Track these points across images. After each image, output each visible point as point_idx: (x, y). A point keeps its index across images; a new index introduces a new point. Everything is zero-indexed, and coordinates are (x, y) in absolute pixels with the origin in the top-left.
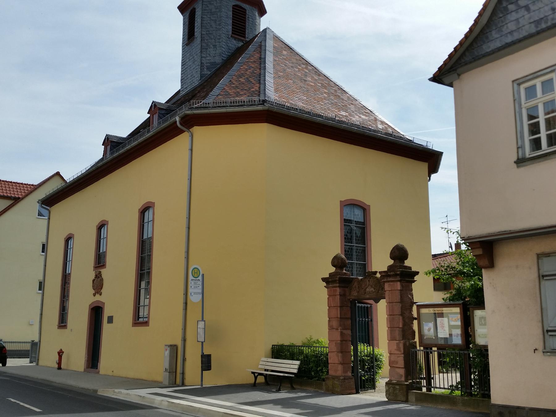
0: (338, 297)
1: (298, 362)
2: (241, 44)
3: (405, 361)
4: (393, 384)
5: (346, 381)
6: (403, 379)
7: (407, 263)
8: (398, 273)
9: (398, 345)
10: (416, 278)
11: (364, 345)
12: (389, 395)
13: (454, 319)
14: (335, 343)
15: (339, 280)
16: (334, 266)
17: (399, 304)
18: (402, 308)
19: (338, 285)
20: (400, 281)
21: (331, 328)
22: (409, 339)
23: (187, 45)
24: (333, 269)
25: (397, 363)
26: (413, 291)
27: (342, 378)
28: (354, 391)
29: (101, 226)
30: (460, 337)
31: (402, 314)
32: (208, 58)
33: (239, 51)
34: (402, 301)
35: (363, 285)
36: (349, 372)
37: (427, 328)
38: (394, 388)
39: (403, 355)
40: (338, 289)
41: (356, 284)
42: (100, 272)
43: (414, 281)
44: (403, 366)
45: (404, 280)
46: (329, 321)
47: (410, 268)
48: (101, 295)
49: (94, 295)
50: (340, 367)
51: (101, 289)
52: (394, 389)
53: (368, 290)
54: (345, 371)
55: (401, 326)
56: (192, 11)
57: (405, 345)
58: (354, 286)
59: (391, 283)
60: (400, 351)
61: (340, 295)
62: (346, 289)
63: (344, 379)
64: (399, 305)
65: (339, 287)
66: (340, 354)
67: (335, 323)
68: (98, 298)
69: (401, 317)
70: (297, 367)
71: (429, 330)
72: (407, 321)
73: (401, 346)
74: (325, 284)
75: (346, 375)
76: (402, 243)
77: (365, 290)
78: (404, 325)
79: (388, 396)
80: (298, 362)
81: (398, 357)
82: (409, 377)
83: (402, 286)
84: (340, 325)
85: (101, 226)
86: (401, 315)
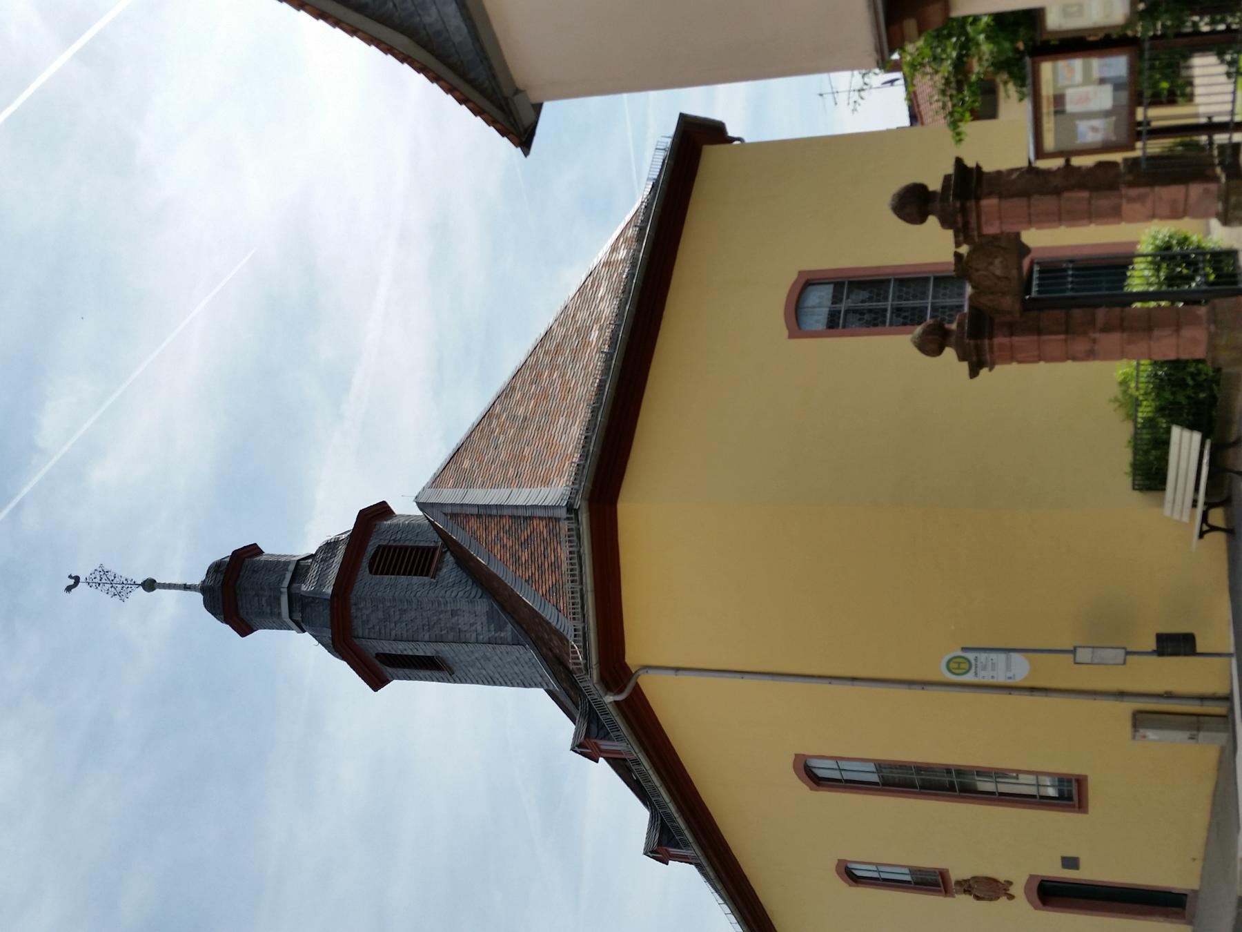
0: (1015, 339)
1: (1176, 431)
2: (449, 557)
4: (1226, 210)
6: (1213, 187)
7: (935, 185)
8: (958, 205)
9: (1131, 200)
16: (938, 351)
18: (1041, 193)
20: (978, 199)
21: (1090, 355)
23: (452, 673)
29: (850, 875)
32: (479, 628)
33: (465, 562)
39: (1157, 189)
42: (958, 883)
43: (978, 168)
46: (1074, 359)
48: (1010, 883)
49: (1011, 897)
50: (1187, 333)
51: (995, 881)
53: (998, 272)
56: (381, 662)
57: (1131, 185)
66: (1156, 333)
67: (1080, 346)
68: (1018, 889)
69: (1066, 195)
70: (1186, 433)
71: (1094, 129)
73: (1133, 192)
74: (984, 372)
78: (1081, 186)
80: (1176, 431)
85: (850, 875)
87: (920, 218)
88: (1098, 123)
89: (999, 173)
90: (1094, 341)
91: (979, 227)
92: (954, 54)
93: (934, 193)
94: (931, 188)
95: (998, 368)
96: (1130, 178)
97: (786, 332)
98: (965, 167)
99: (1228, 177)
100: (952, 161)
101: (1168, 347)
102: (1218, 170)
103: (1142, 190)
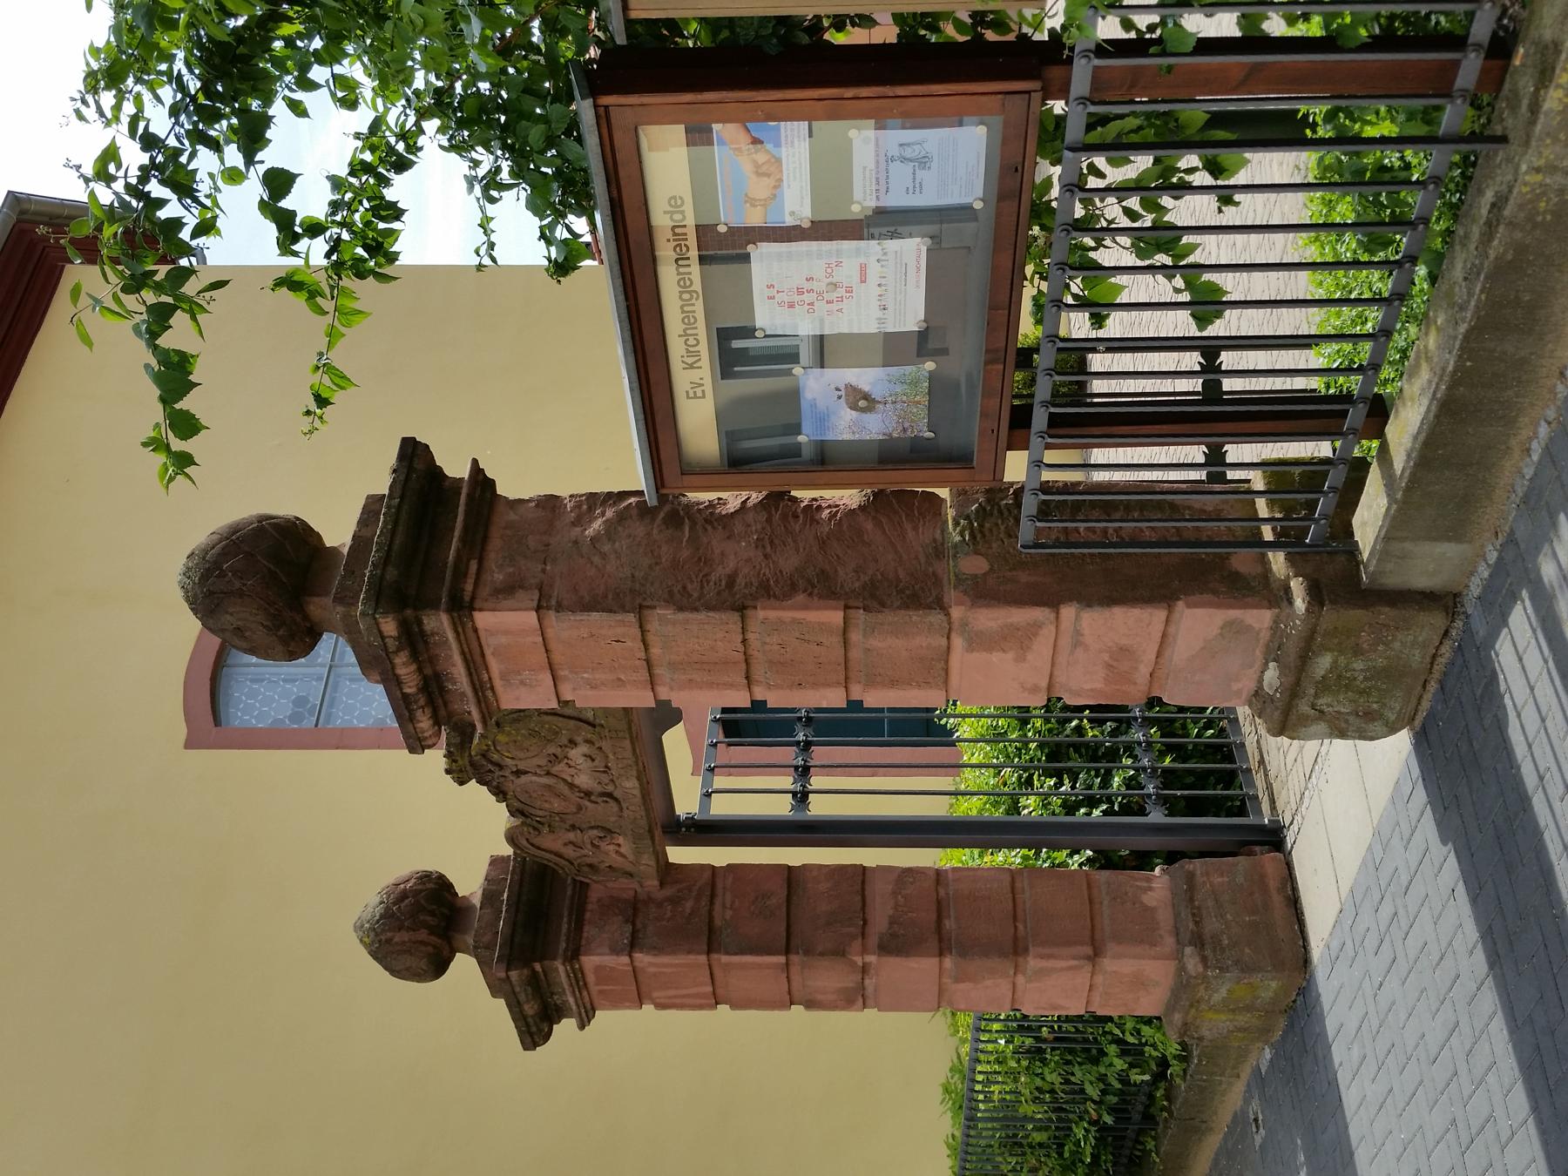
0: (642, 958)
3: (1110, 601)
4: (1293, 692)
5: (1211, 925)
6: (1260, 619)
7: (337, 529)
8: (390, 627)
9: (980, 642)
10: (455, 467)
11: (893, 348)
12: (1369, 716)
13: (760, 189)
14: (958, 980)
15: (526, 962)
16: (438, 967)
17: (653, 625)
18: (683, 602)
19: (560, 969)
20: (462, 608)
21: (855, 997)
22: (938, 550)
24: (464, 967)
25: (1124, 652)
26: (563, 491)
27: (1193, 964)
28: (1269, 861)
30: (932, 139)
31: (736, 601)
34: (630, 600)
35: (557, 805)
36: (1150, 899)
37: (848, 415)
38: (1323, 686)
39: (1068, 612)
40: (589, 962)
41: (548, 841)
43: (481, 482)
44: (1157, 616)
45: (460, 574)
46: (810, 1004)
47: (372, 506)
50: (1119, 965)
52: (1337, 682)
53: (584, 780)
54: (1141, 933)
55: (836, 617)
57: (983, 593)
58: (569, 852)
59: (495, 666)
60: (1036, 627)
61: (633, 945)
62: (596, 893)
63: (1198, 941)
64: (663, 620)
65: (574, 955)
66: (1033, 963)
67: (828, 977)
69: (763, 614)
71: (861, 400)
72: (788, 561)
73: (990, 619)
74: (565, 1029)
75: (1165, 917)
76: (179, 562)
77: (588, 794)
78: (819, 585)
79: (1378, 726)
81: (1078, 642)
82: (1242, 560)
83: (508, 590)
84: (839, 952)
86: (741, 609)
87: (296, 638)
88: (867, 378)
89: (550, 503)
90: (865, 969)
91: (482, 689)
92: (1493, 556)
93: (334, 551)
94: (330, 541)
95: (604, 1018)
96: (975, 565)
97: (182, 731)
98: (436, 473)
99: (1316, 593)
100: (391, 456)
101: (1057, 989)
102: (1278, 561)
103: (1021, 616)
